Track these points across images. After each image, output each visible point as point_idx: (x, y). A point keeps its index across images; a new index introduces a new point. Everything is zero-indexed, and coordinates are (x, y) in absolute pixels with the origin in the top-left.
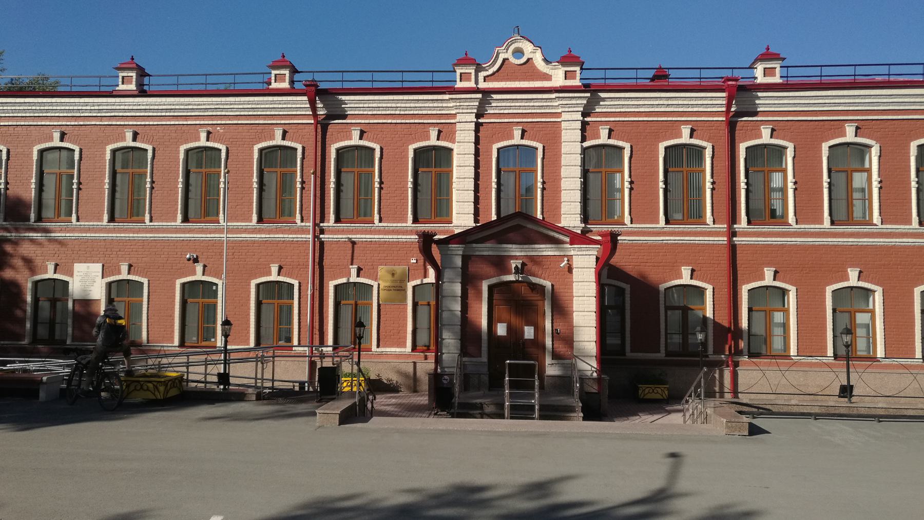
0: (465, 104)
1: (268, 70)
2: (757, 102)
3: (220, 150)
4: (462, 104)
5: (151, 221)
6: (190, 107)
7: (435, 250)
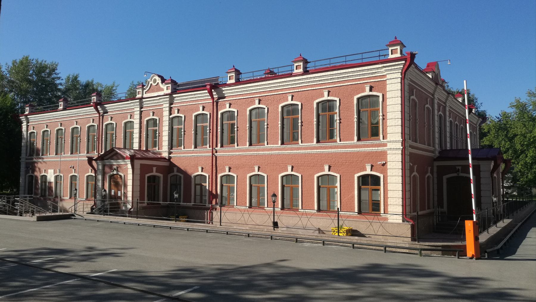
0: (136, 104)
1: (386, 48)
2: (224, 92)
3: (182, 117)
4: (135, 104)
5: (267, 144)
6: (72, 113)
7: (94, 163)
